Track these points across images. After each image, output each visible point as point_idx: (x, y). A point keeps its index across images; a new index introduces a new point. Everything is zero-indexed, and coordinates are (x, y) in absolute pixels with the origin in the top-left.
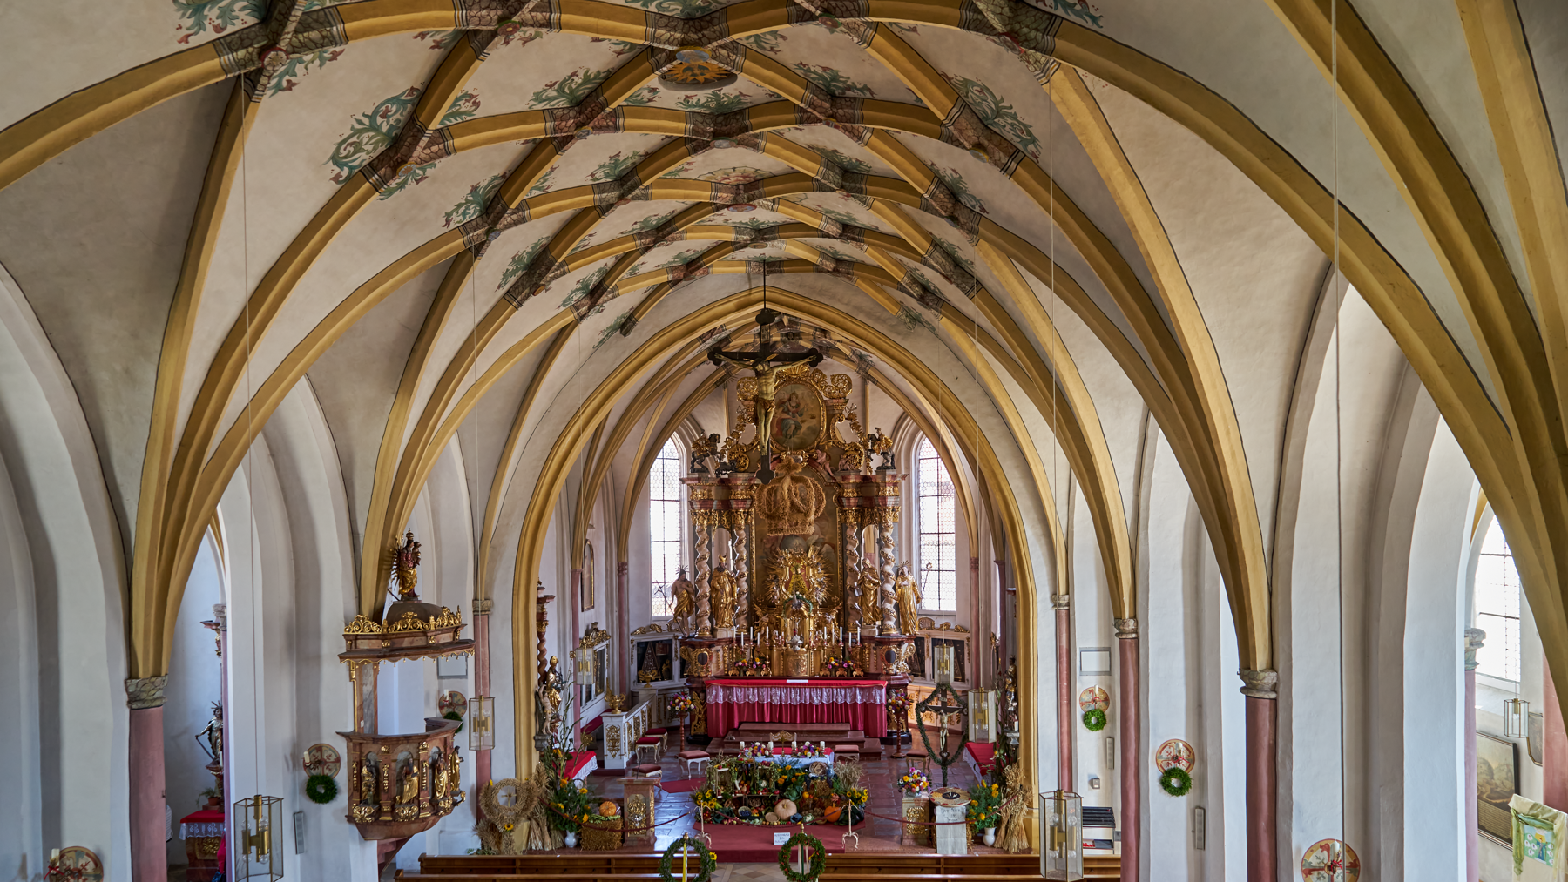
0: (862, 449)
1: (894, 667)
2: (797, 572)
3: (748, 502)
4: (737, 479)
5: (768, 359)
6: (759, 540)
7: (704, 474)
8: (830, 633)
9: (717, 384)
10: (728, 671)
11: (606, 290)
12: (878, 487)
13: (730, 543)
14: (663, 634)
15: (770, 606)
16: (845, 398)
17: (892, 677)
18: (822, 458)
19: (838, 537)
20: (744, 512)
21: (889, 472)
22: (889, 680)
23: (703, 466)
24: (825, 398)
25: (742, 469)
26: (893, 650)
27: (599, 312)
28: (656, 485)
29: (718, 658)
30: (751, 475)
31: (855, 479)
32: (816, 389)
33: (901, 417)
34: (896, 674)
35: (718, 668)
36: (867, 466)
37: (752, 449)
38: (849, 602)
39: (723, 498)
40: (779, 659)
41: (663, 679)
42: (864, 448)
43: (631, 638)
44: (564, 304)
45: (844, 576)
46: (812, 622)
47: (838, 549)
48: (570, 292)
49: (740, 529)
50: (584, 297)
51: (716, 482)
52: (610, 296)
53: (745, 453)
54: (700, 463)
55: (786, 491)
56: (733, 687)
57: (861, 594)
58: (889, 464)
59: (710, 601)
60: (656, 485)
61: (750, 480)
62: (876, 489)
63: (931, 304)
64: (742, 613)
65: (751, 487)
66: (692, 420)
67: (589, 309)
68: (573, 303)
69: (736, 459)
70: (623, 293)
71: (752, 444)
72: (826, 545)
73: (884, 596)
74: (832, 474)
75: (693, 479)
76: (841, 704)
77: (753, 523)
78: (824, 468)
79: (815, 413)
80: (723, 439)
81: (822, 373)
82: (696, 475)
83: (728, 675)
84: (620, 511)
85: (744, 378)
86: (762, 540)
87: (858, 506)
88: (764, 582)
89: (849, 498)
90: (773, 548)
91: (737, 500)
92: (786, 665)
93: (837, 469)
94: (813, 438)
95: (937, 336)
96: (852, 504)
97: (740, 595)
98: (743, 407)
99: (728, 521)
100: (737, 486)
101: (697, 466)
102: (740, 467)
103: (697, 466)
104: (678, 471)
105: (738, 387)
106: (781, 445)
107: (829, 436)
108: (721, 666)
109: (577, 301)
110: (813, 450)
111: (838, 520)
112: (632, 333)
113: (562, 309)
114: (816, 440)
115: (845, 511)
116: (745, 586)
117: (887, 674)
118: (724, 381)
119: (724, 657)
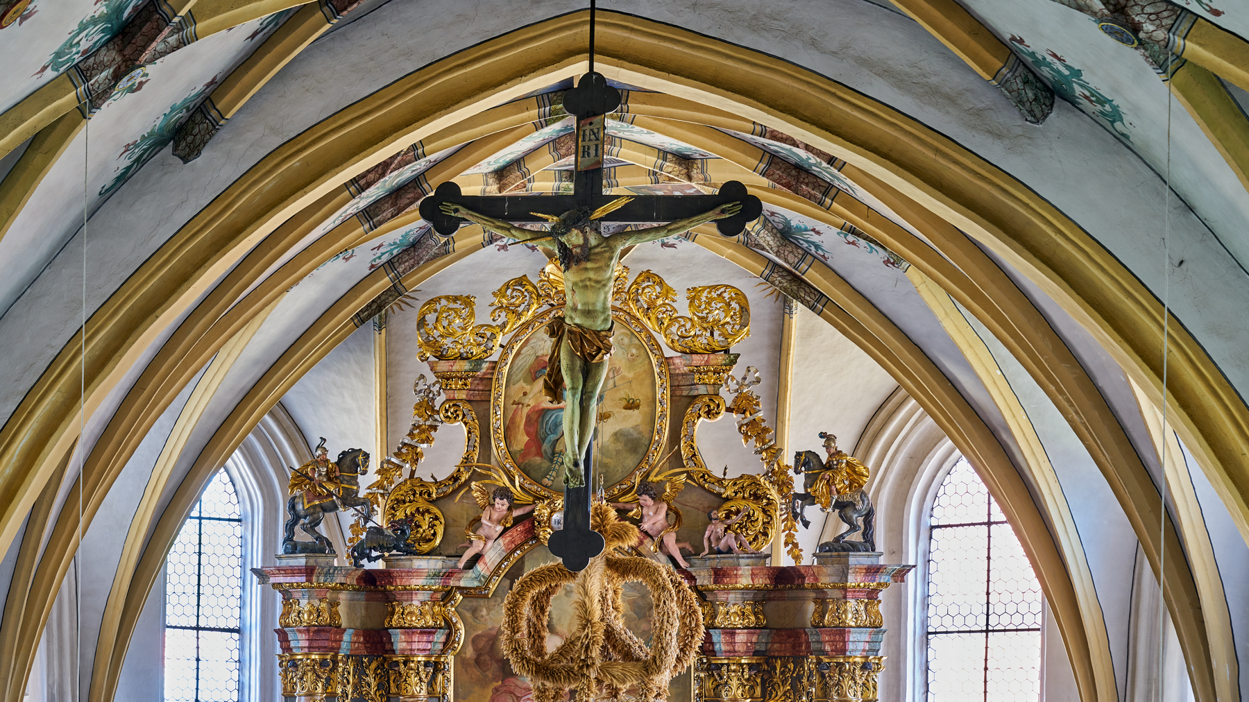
0: (774, 494)
3: (440, 637)
4: (411, 573)
5: (598, 213)
7: (322, 560)
9: (361, 319)
11: (167, 22)
12: (822, 601)
16: (727, 351)
20: (427, 664)
21: (857, 560)
23: (320, 538)
24: (668, 353)
25: (426, 547)
27: (132, 90)
28: (179, 589)
30: (451, 563)
31: (753, 575)
32: (644, 328)
33: (881, 407)
36: (791, 543)
37: (455, 492)
39: (369, 625)
42: (780, 491)
44: (55, 64)
48: (75, 27)
50: (108, 41)
51: (352, 581)
52: (172, 40)
53: (433, 502)
54: (311, 528)
55: (597, 598)
58: (856, 537)
60: (179, 589)
61: (449, 575)
62: (811, 607)
63: (1148, 27)
65: (447, 596)
66: (282, 415)
67: (117, 77)
68: (77, 58)
69: (409, 519)
70: (206, 33)
71: (454, 478)
74: (683, 564)
75: (292, 571)
78: (661, 546)
79: (640, 393)
80: (374, 464)
81: (661, 283)
82: (300, 561)
85: (437, 300)
87: (756, 653)
89: (731, 632)
91: (409, 630)
93: (698, 550)
94: (630, 461)
95: (1122, 139)
96: (740, 648)
98: (431, 378)
99: (379, 687)
100: (410, 592)
101: (301, 536)
102: (418, 541)
103: (301, 536)
104: (238, 552)
105: (422, 323)
106: (538, 481)
107: (676, 459)
109: (88, 54)
110: (629, 497)
112: (206, 153)
113: (50, 74)
114: (638, 467)
115: (720, 666)
118: (380, 308)
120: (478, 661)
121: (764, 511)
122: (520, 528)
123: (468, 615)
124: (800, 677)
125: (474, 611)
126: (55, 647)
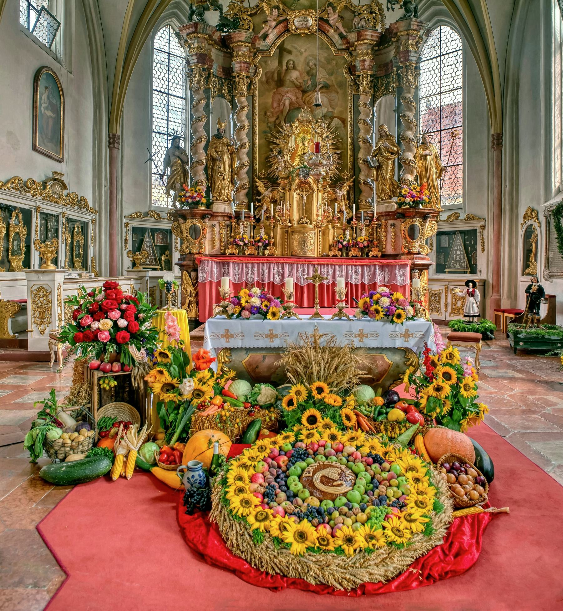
1: (417, 244)
2: (304, 144)
6: (263, 113)
8: (341, 211)
10: (225, 250)
13: (231, 116)
14: (161, 222)
15: (272, 182)
17: (415, 256)
18: (333, 18)
19: (349, 110)
20: (247, 77)
22: (413, 259)
26: (418, 224)
29: (213, 234)
34: (419, 253)
35: (213, 247)
38: (362, 177)
40: (283, 238)
41: (162, 269)
43: (124, 221)
45: (356, 150)
46: (320, 194)
47: (349, 123)
49: (241, 94)
56: (228, 264)
57: (377, 164)
59: (206, 169)
64: (242, 187)
72: (336, 119)
73: (403, 164)
76: (357, 286)
77: (257, 93)
83: (225, 253)
84: (112, 77)
86: (265, 113)
88: (267, 158)
90: (278, 122)
92: (290, 245)
96: (366, 67)
97: (240, 167)
108: (217, 243)
111: (349, 91)
116: (246, 159)
117: (409, 253)
119: (220, 234)
120: (267, 82)
121: (374, 18)
122: (282, 25)
123: (263, 64)
124: (388, 83)
125: (265, 62)
126: (96, 71)
